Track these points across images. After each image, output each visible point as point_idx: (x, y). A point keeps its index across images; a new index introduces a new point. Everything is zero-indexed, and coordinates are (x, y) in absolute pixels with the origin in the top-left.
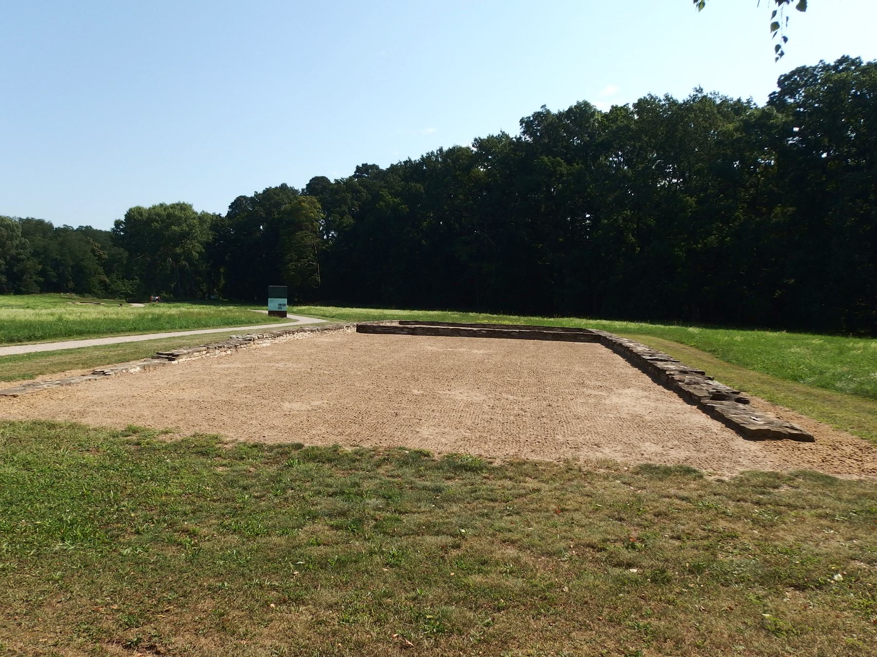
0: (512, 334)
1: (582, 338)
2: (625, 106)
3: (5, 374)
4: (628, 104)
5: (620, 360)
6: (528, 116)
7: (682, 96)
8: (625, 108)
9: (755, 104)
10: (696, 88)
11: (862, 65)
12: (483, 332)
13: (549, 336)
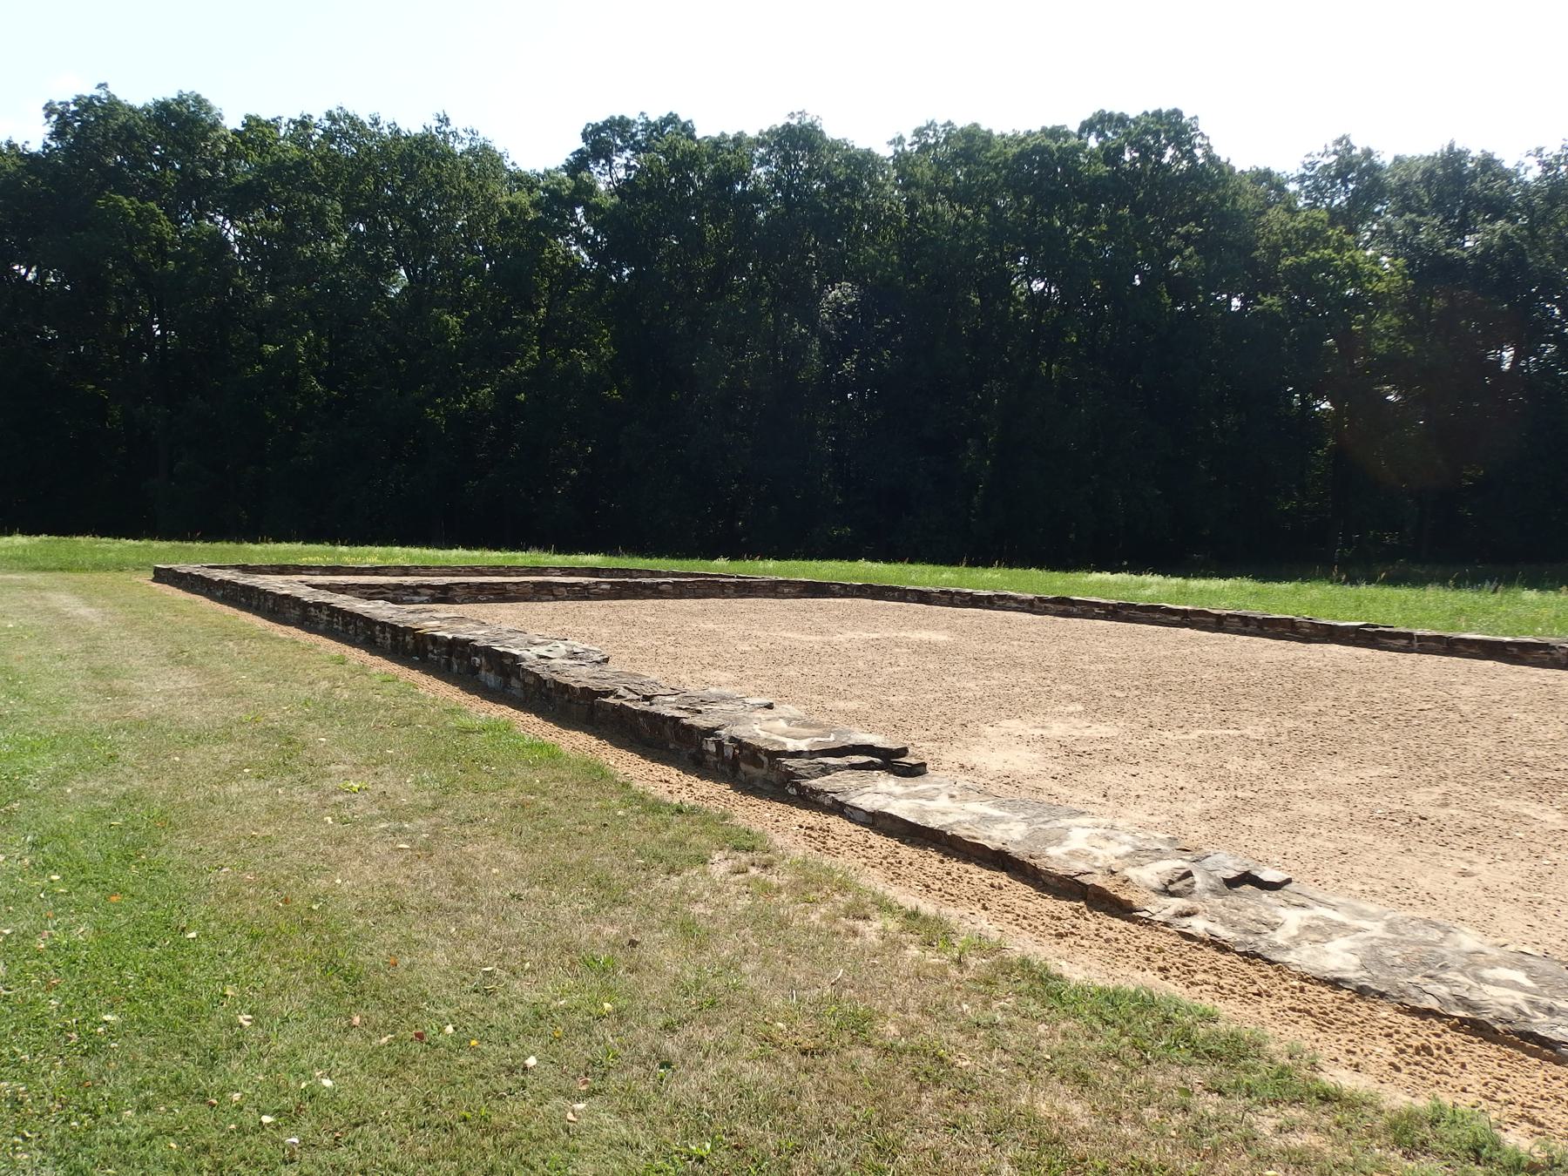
0: (660, 588)
1: (786, 590)
2: (274, 120)
3: (1531, 1077)
4: (280, 118)
5: (203, 602)
6: (64, 100)
7: (413, 125)
8: (273, 125)
9: (513, 164)
10: (439, 116)
11: (1354, 152)
12: (604, 586)
13: (729, 588)
